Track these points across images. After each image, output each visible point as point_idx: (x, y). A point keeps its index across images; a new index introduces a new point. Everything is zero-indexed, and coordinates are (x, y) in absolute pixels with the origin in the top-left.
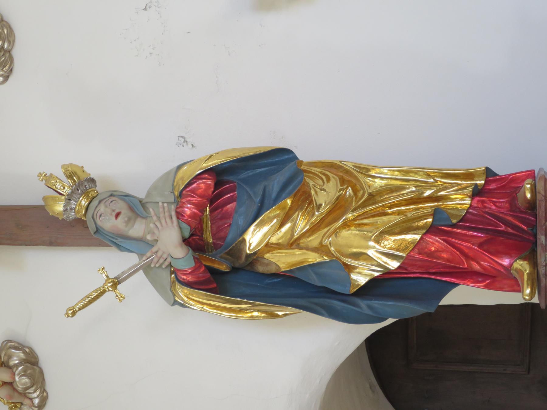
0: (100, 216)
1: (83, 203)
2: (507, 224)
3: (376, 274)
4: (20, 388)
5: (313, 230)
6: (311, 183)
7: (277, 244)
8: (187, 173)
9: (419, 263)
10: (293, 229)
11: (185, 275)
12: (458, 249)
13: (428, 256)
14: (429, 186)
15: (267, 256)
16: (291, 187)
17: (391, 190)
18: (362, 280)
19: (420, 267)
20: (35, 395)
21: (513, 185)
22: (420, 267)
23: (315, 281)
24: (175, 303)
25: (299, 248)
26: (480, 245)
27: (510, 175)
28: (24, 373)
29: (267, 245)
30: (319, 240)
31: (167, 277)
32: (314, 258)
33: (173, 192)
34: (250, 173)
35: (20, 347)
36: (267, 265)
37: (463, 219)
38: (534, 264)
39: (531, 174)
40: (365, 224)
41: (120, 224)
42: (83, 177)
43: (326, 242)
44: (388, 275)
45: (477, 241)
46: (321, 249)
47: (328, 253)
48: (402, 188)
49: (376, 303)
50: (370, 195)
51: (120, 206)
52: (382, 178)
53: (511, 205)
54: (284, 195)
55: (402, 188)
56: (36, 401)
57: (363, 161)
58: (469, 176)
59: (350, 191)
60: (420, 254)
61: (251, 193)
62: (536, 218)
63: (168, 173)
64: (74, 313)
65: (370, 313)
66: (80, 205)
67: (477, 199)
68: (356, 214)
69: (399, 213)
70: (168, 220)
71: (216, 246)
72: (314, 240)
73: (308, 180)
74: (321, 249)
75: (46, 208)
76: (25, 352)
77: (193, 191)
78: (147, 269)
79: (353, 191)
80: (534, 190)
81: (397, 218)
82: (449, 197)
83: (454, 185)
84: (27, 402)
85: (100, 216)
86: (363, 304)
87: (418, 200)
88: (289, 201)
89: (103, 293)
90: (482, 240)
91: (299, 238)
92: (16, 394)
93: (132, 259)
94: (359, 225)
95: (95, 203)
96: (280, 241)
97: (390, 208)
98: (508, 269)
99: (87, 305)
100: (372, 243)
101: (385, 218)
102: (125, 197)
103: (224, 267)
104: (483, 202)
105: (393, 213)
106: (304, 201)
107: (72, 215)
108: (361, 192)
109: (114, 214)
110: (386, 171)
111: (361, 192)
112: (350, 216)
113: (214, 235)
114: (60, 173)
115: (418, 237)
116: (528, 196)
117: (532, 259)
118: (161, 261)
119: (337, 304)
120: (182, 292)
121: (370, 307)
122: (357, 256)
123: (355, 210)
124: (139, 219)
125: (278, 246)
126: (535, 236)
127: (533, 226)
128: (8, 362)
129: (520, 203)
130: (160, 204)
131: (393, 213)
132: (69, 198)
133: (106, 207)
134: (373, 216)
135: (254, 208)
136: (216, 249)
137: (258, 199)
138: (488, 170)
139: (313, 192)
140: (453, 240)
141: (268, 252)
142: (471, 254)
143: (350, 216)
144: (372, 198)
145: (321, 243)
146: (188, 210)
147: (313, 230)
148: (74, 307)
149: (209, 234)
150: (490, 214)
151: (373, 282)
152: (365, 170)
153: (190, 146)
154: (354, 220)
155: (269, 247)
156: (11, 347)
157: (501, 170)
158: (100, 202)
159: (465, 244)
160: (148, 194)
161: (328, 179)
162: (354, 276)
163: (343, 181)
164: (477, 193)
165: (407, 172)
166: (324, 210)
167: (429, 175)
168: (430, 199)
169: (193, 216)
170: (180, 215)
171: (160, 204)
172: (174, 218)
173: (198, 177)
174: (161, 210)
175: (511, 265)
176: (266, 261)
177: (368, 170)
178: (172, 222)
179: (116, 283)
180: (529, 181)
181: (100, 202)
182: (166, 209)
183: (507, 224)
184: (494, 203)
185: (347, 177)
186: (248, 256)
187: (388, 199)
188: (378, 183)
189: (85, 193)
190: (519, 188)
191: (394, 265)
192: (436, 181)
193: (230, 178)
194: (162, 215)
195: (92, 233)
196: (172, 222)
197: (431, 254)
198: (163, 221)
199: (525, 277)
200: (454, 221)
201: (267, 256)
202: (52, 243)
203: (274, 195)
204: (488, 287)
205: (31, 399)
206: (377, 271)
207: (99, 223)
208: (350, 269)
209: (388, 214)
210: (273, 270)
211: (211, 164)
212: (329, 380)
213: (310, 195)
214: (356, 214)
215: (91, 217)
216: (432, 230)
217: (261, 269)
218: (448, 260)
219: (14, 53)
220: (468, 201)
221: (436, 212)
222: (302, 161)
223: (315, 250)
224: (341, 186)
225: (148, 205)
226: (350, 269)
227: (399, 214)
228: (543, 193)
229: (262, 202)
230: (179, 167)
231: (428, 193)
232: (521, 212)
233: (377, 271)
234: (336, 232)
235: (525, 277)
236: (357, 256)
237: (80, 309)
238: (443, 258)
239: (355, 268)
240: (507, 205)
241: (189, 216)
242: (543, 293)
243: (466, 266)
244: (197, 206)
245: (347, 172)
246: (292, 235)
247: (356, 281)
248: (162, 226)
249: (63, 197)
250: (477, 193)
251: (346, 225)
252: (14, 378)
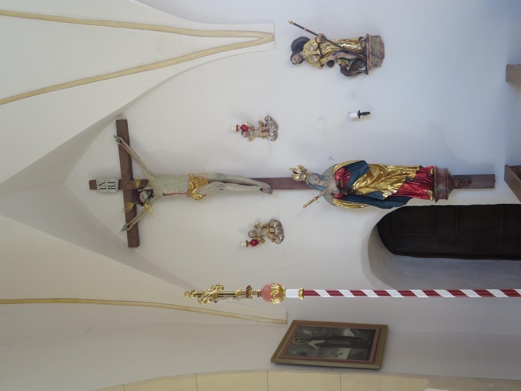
0: (311, 180)
1: (305, 176)
2: (426, 181)
3: (390, 194)
4: (277, 234)
5: (372, 183)
6: (372, 170)
7: (362, 187)
8: (337, 168)
9: (402, 191)
10: (367, 183)
11: (336, 195)
12: (414, 188)
13: (404, 189)
14: (404, 171)
15: (359, 190)
16: (366, 171)
17: (394, 172)
18: (386, 196)
19: (402, 192)
20: (281, 236)
21: (428, 170)
22: (402, 192)
23: (373, 197)
24: (332, 204)
25: (368, 188)
26: (418, 186)
27: (427, 167)
28: (278, 229)
29: (359, 187)
30: (374, 186)
31: (330, 197)
32: (372, 190)
33: (332, 173)
34: (354, 168)
35: (276, 221)
36: (359, 193)
37: (414, 179)
38: (433, 191)
39: (433, 167)
40: (387, 181)
41: (317, 182)
42: (304, 169)
43: (376, 186)
44: (393, 194)
45: (418, 185)
46: (374, 188)
47: (377, 189)
48: (397, 171)
49: (389, 203)
50: (388, 173)
51: (316, 177)
52: (391, 169)
53: (427, 176)
54: (364, 174)
55: (397, 171)
56: (281, 238)
57: (386, 164)
58: (415, 168)
59: (382, 172)
60: (402, 189)
61: (355, 173)
62: (434, 179)
63: (330, 168)
64: (306, 206)
65: (388, 205)
66: (304, 177)
67: (417, 174)
68: (384, 178)
69: (396, 178)
70: (333, 180)
71: (344, 188)
72: (373, 186)
73: (370, 169)
74: (374, 188)
75: (293, 178)
76: (278, 223)
77: (339, 172)
78: (324, 195)
79: (383, 172)
80: (433, 172)
81: (396, 179)
82: (356, 351)
83: (411, 170)
84: (278, 238)
85: (311, 180)
86: (386, 203)
87: (401, 174)
88: (366, 175)
89: (314, 200)
90: (419, 185)
91: (368, 185)
92: (275, 236)
93: (316, 193)
94: (385, 181)
95: (308, 176)
96: (363, 186)
97: (394, 177)
98: (426, 192)
99: (309, 204)
100: (389, 186)
101: (392, 179)
102: (317, 174)
103: (346, 194)
104: (419, 175)
105: (394, 178)
106: (370, 175)
107: (301, 180)
108: (386, 172)
109: (315, 179)
110: (392, 166)
111: (386, 172)
112: (383, 179)
113: (343, 185)
114: (298, 168)
115: (402, 184)
116: (432, 173)
117: (433, 190)
118: (329, 192)
119: (379, 203)
120: (335, 201)
121: (388, 204)
122: (384, 189)
123: (384, 177)
124: (322, 181)
125: (362, 187)
126: (434, 184)
127: (433, 181)
128: (273, 226)
129: (429, 175)
130: (330, 176)
131: (394, 178)
132: (301, 175)
133: (312, 177)
134: (389, 179)
135: (356, 177)
136: (344, 189)
137: (357, 175)
138: (420, 166)
139: (372, 172)
140: (411, 185)
141: (360, 189)
142: (416, 189)
143: (383, 179)
144: (389, 174)
145: (375, 186)
146: (338, 177)
147: (372, 183)
148: (305, 205)
149: (342, 185)
150: (421, 178)
151: (389, 197)
152: (386, 166)
153: (333, 160)
154: (384, 180)
155: (360, 188)
156: (274, 221)
157: (424, 166)
158: (310, 176)
159: (414, 186)
160: (324, 173)
161: (376, 169)
162: (384, 195)
163: (380, 170)
164: (417, 172)
165: (398, 167)
166: (375, 177)
167: (404, 168)
168: (405, 174)
169: (339, 179)
170: (336, 179)
171: (330, 176)
172: (334, 180)
173: (340, 169)
174: (331, 178)
175: (427, 192)
176: (359, 192)
177: (387, 166)
178: (334, 181)
179: (317, 198)
180: (432, 169)
181: (310, 176)
182: (332, 177)
183: (426, 181)
184: (422, 175)
185: (381, 169)
186: (354, 190)
187: (393, 174)
188: (390, 170)
189: (305, 174)
190: (429, 171)
191: (395, 191)
192: (406, 169)
193: (348, 169)
194: (331, 179)
195: (308, 184)
196: (334, 181)
197: (405, 189)
198: (331, 181)
199: (431, 194)
200: (411, 180)
201: (359, 190)
202: (291, 189)
203: (361, 174)
204: (420, 198)
205: (279, 238)
206: (390, 194)
207: (310, 182)
208: (383, 193)
209: (393, 178)
210: (361, 194)
211: (344, 165)
212: (369, 236)
213: (372, 174)
214: (384, 178)
215: (307, 180)
216: (405, 182)
217: (357, 194)
218: (410, 190)
219: (278, 132)
220: (415, 175)
221: (406, 178)
222: (369, 164)
223: (373, 188)
224: (380, 171)
225: (324, 177)
226: (383, 193)
227: (396, 178)
228: (436, 172)
229: (358, 175)
230: (334, 166)
231: (404, 172)
232: (430, 177)
233: (390, 194)
234: (379, 183)
235: (431, 194)
236: (384, 189)
237: (308, 205)
238: (408, 190)
239: (384, 193)
240: (426, 176)
241: (338, 179)
242: (436, 199)
243: (415, 192)
244: (340, 176)
245: (381, 167)
246: (367, 184)
247: (384, 196)
248: (331, 182)
249: (299, 175)
250: (417, 172)
251: (382, 181)
252: (275, 231)
